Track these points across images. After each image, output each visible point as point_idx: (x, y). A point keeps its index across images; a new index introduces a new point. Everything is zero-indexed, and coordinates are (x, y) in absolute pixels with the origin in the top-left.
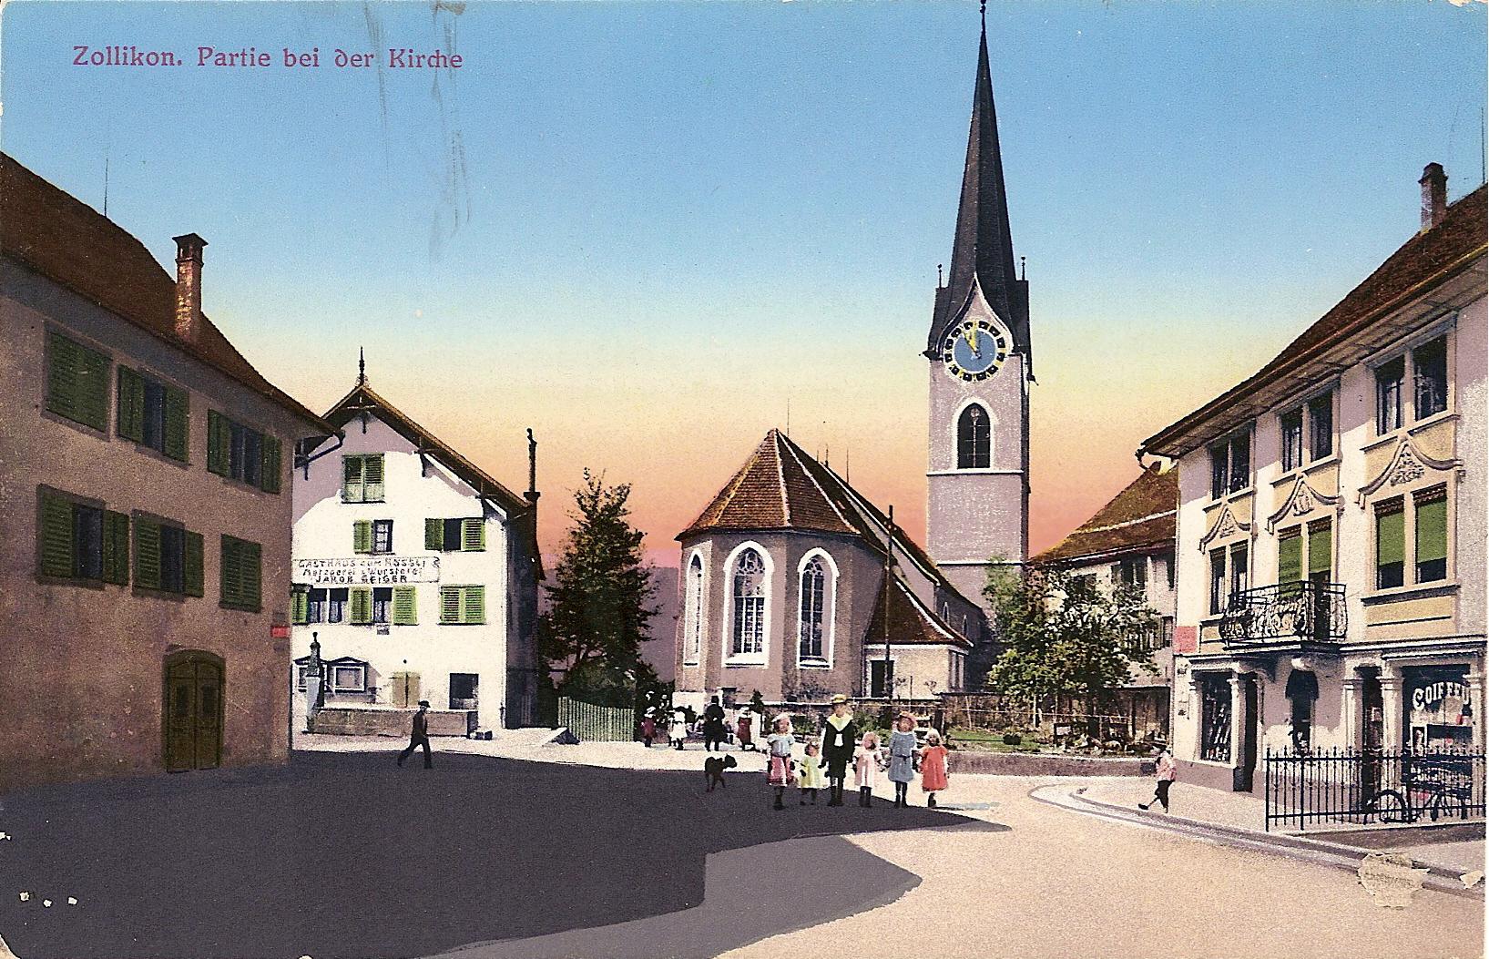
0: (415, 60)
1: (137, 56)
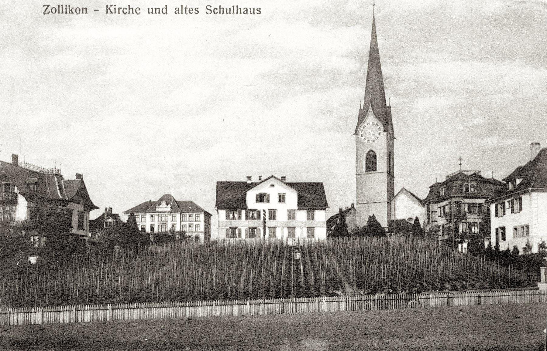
0: (117, 10)
1: (71, 9)
